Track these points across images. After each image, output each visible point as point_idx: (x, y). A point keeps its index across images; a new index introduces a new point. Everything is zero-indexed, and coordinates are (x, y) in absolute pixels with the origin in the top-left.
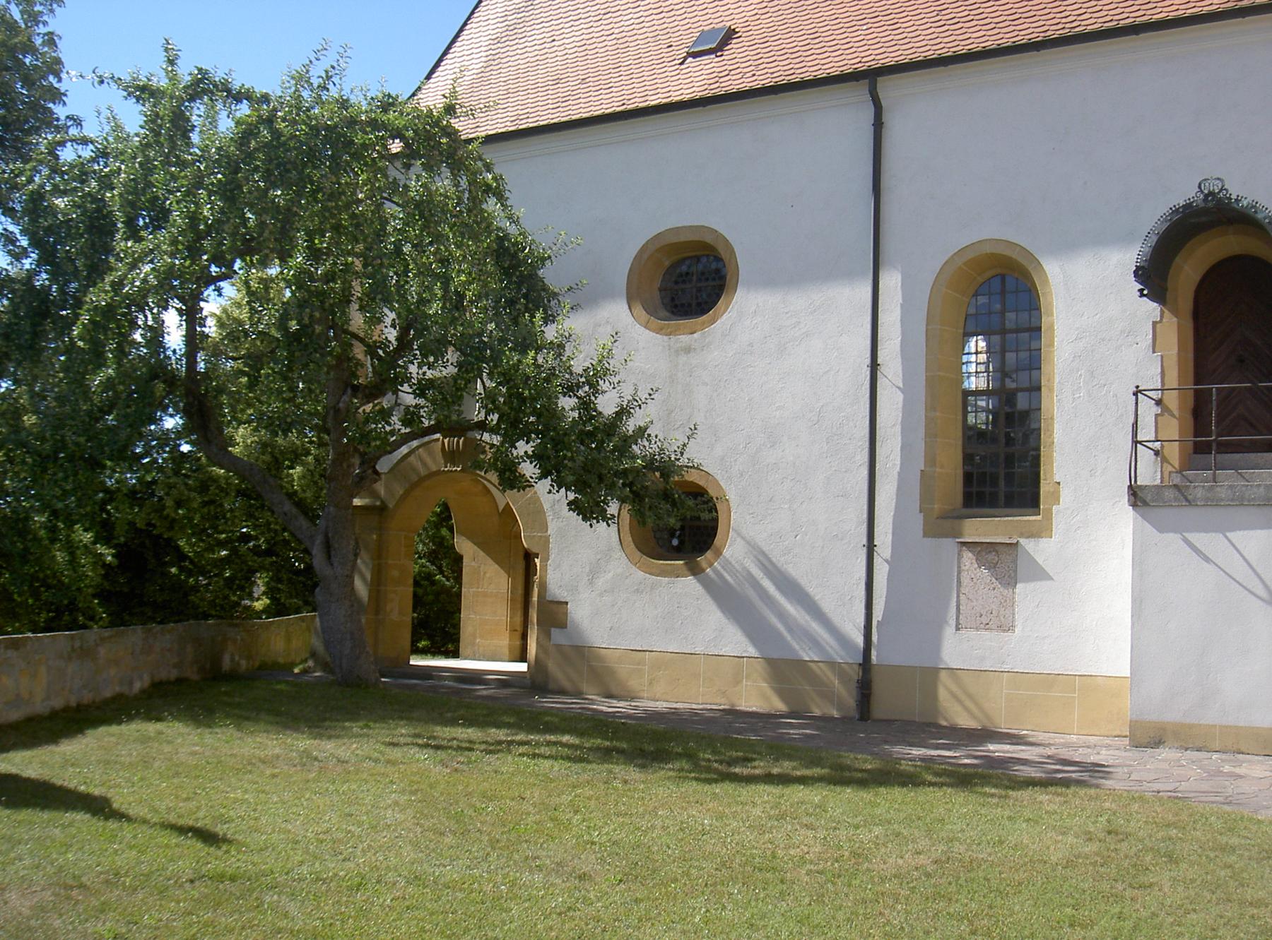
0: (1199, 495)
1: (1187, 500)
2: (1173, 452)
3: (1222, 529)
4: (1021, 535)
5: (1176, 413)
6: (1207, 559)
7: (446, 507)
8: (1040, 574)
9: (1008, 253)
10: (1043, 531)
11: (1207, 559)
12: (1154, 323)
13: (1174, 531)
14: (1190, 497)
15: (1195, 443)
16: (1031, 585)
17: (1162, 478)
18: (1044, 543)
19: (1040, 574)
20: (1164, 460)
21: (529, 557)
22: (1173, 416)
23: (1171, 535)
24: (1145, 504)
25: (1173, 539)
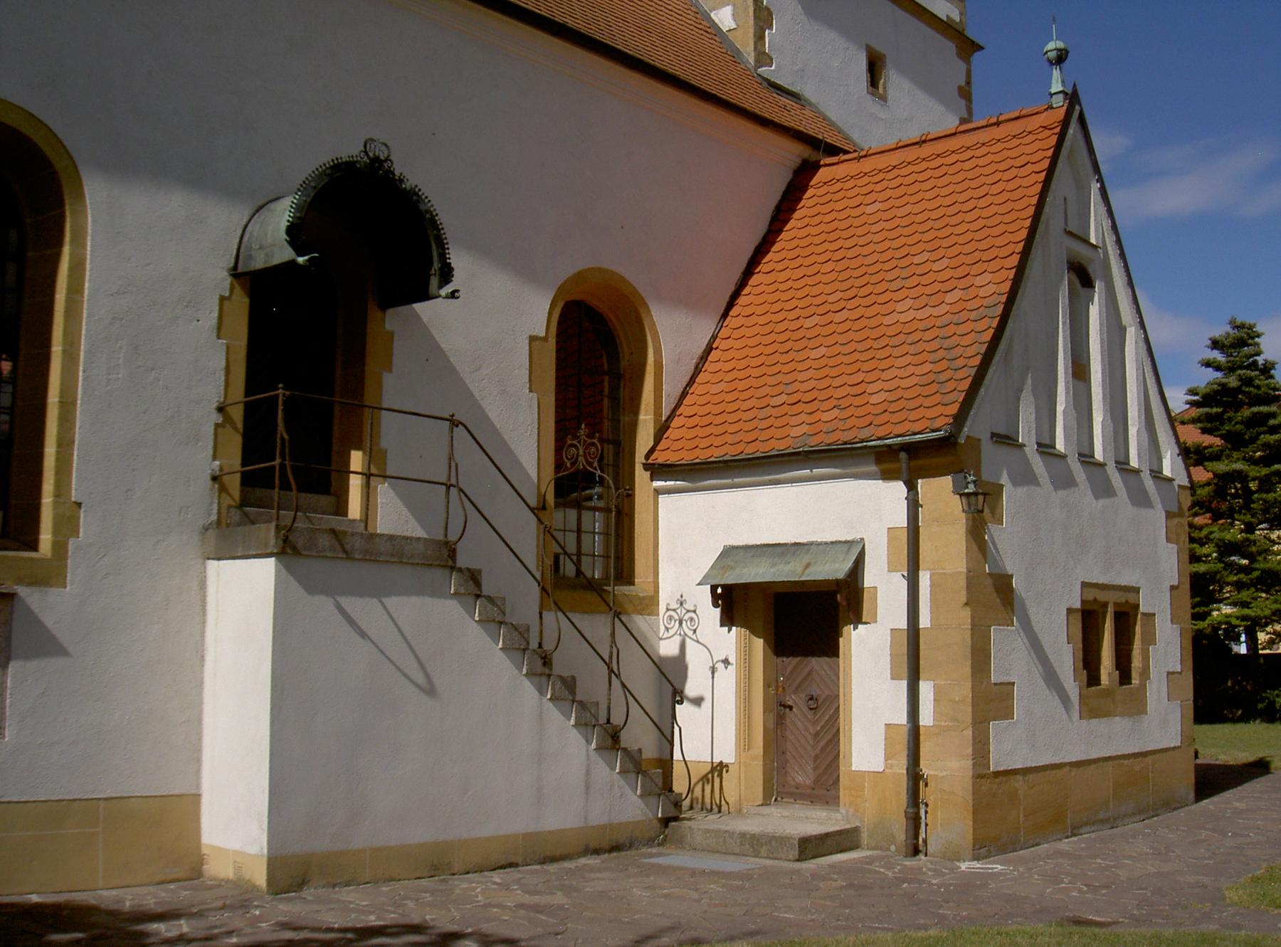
0: (357, 545)
1: (345, 552)
2: (234, 483)
3: (379, 592)
4: (20, 581)
5: (240, 426)
6: (363, 634)
7: (982, 48)
8: (47, 646)
9: (27, 130)
10: (51, 575)
11: (363, 634)
12: (222, 299)
13: (371, 595)
14: (347, 547)
15: (243, 474)
16: (33, 665)
17: (219, 513)
18: (53, 594)
19: (47, 646)
20: (223, 489)
21: (638, 942)
22: (236, 429)
23: (323, 598)
24: (296, 552)
25: (324, 604)
